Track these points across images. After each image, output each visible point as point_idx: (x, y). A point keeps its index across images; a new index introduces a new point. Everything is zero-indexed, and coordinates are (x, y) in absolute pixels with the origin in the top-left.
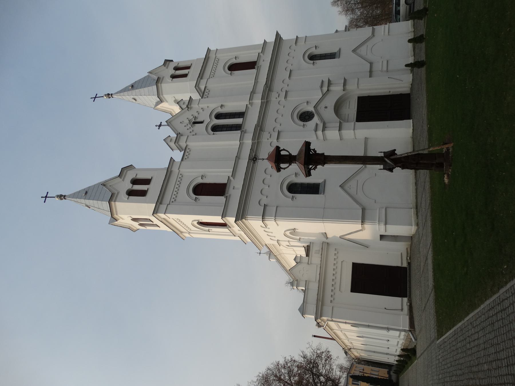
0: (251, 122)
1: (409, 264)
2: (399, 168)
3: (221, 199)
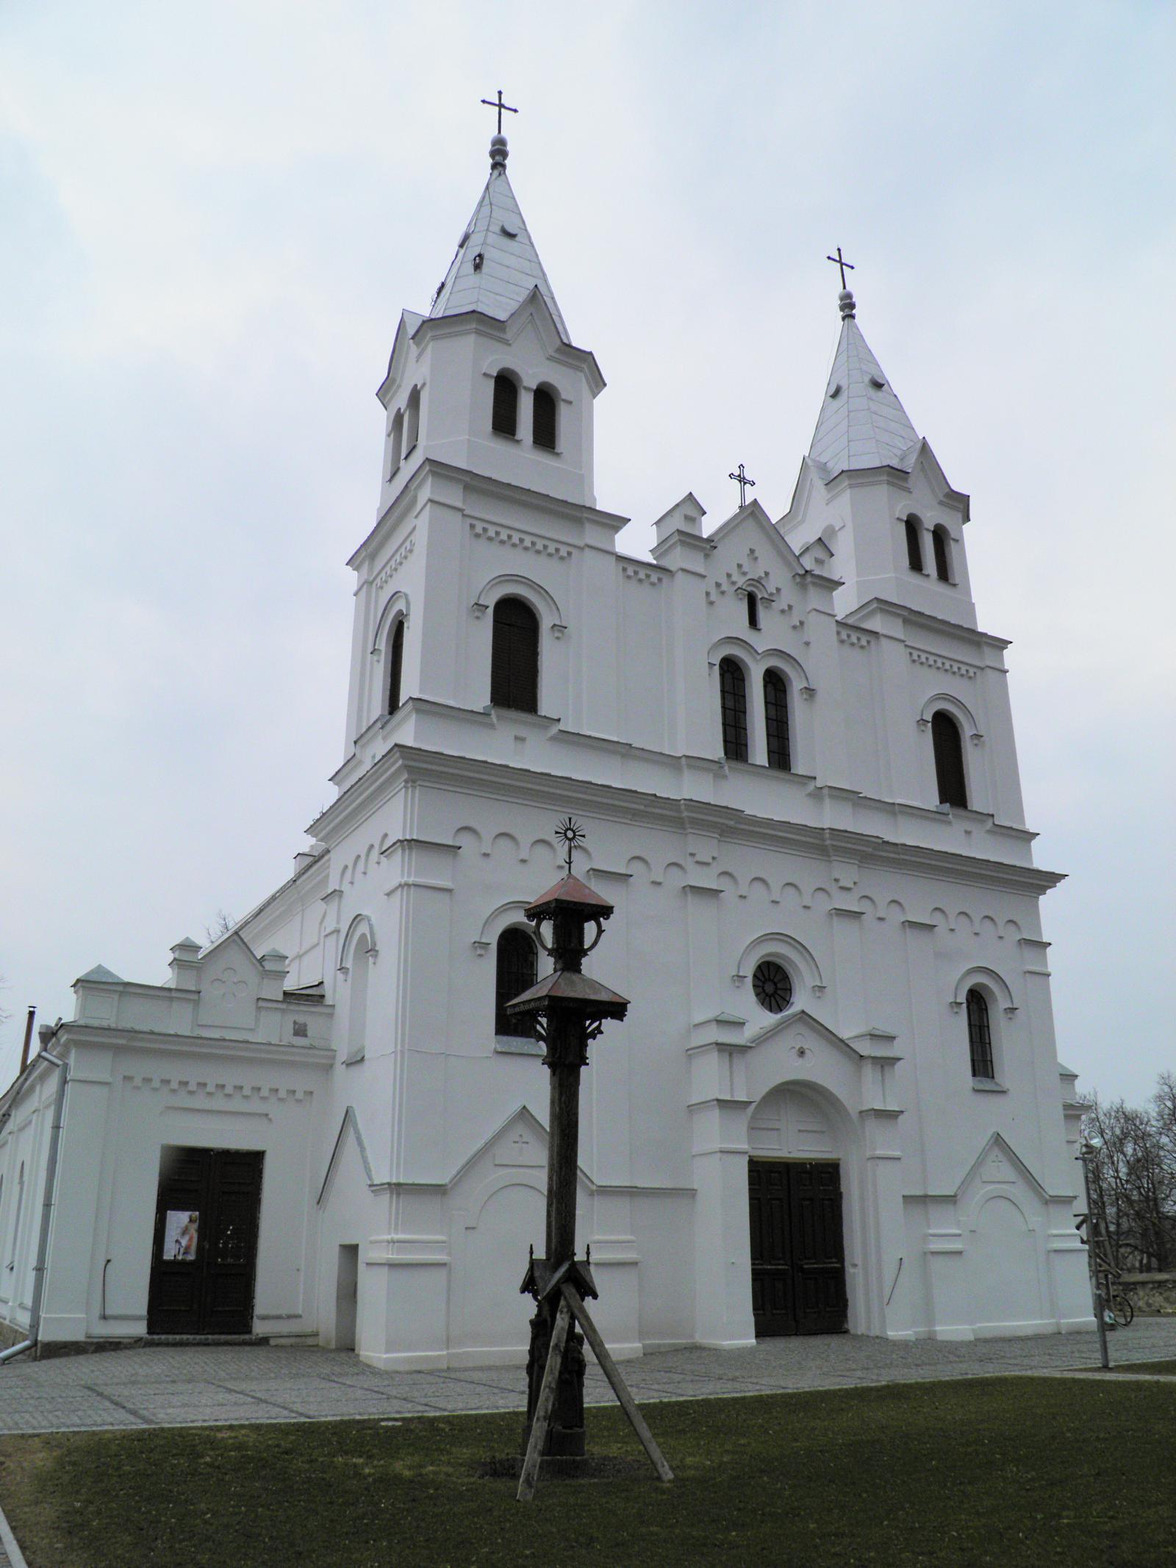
0: (756, 796)
1: (263, 1341)
2: (535, 1311)
3: (479, 694)
